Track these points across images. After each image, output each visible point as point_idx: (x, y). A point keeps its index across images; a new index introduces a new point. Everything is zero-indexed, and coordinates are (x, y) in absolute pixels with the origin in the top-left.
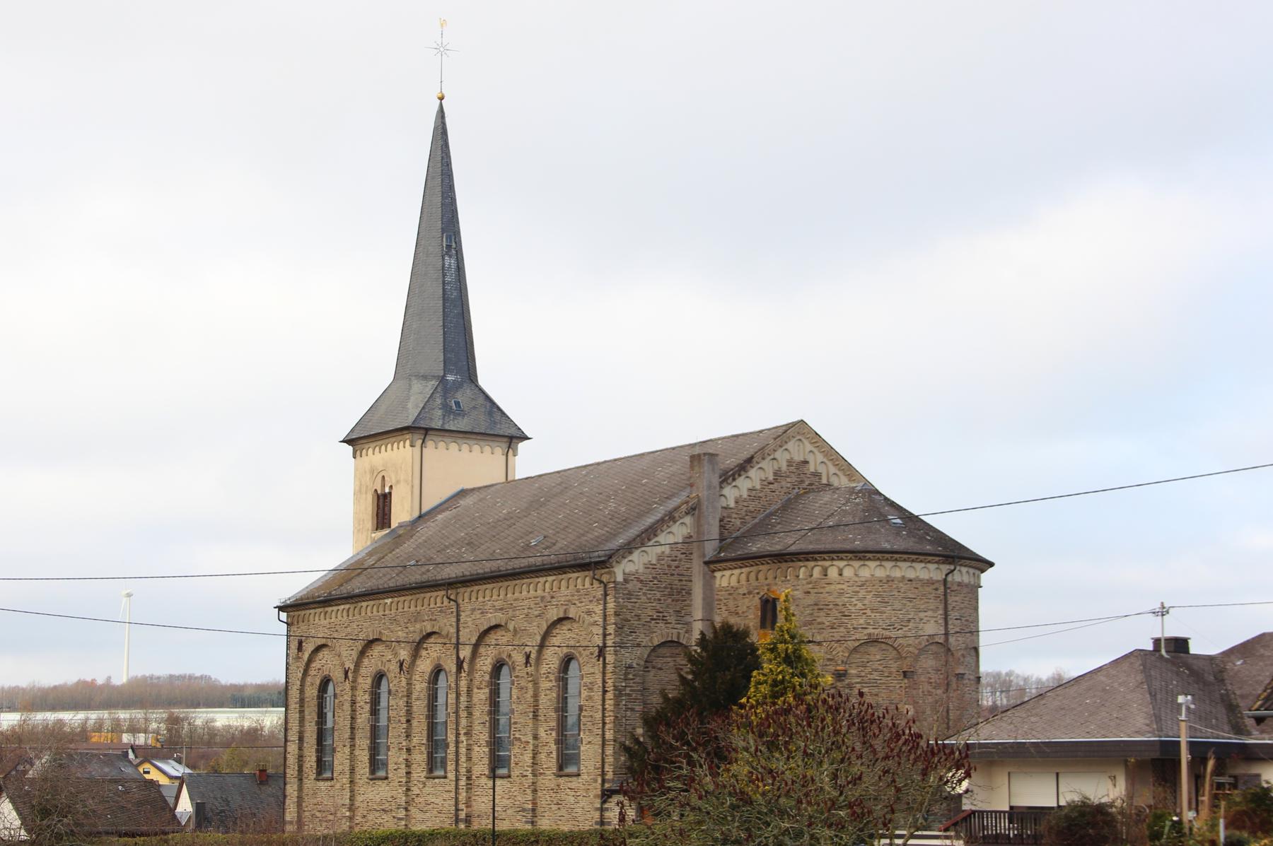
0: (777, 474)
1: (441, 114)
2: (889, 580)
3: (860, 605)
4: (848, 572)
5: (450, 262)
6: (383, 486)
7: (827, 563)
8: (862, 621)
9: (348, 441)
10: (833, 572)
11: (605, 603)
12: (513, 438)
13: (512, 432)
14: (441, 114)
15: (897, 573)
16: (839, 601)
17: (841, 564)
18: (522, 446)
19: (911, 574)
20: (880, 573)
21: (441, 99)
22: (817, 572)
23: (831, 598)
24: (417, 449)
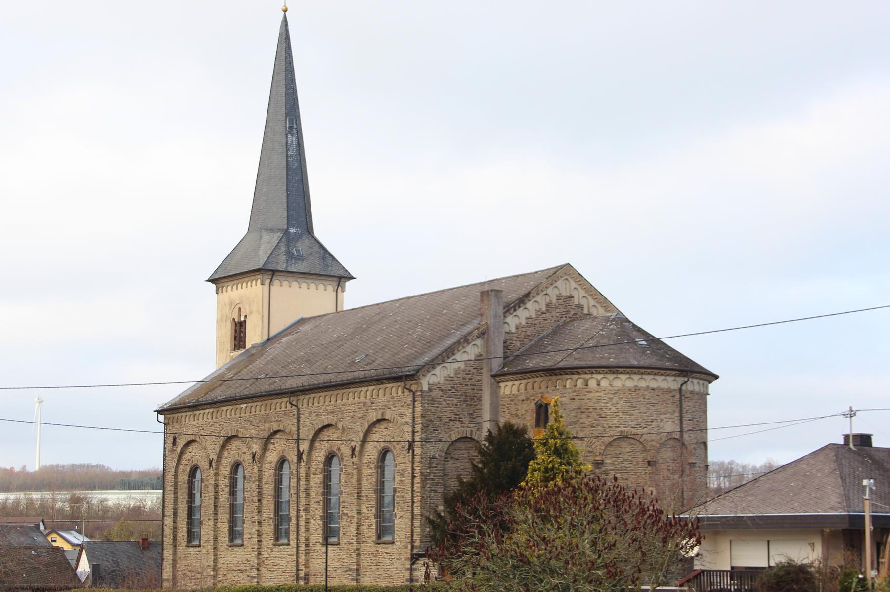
0: (549, 306)
1: (285, 22)
2: (637, 389)
3: (613, 409)
4: (604, 383)
5: (292, 139)
6: (240, 316)
7: (588, 376)
8: (615, 422)
9: (212, 280)
10: (592, 383)
11: (414, 407)
12: (342, 278)
13: (340, 273)
14: (285, 22)
15: (643, 384)
16: (597, 406)
17: (599, 376)
18: (349, 284)
19: (653, 385)
20: (630, 384)
21: (285, 11)
22: (580, 383)
23: (591, 404)
24: (266, 286)
